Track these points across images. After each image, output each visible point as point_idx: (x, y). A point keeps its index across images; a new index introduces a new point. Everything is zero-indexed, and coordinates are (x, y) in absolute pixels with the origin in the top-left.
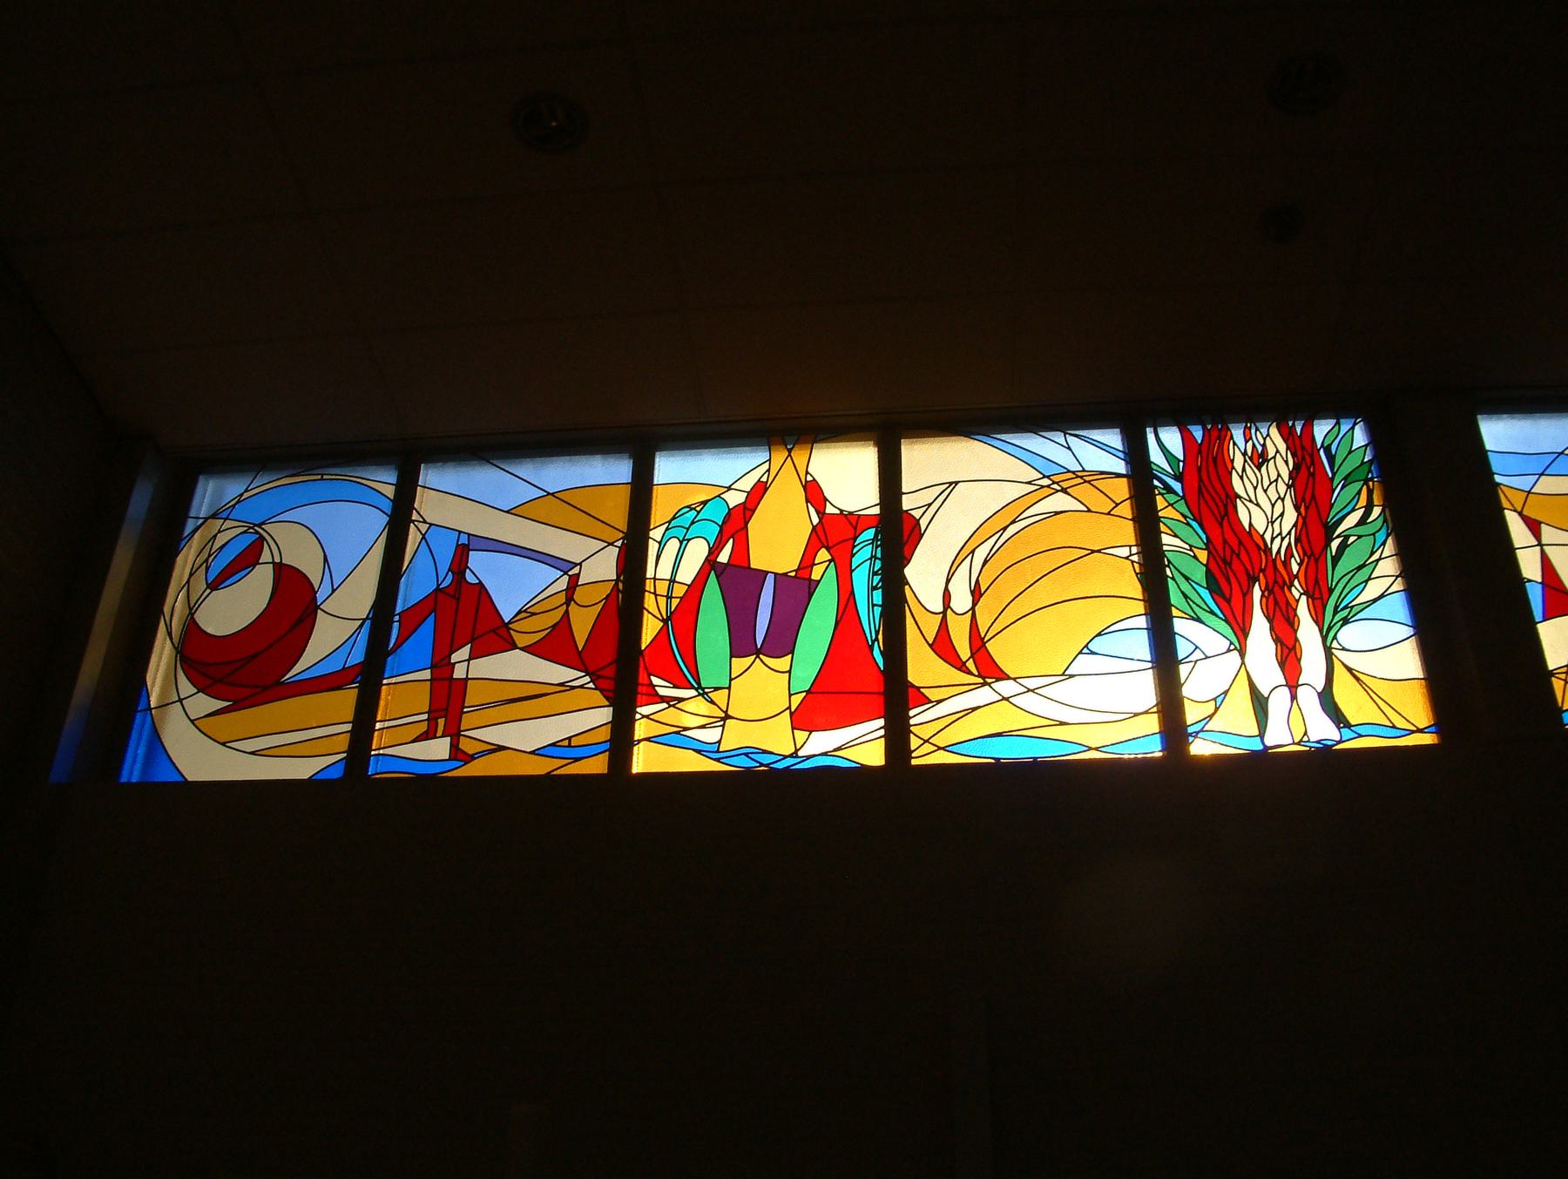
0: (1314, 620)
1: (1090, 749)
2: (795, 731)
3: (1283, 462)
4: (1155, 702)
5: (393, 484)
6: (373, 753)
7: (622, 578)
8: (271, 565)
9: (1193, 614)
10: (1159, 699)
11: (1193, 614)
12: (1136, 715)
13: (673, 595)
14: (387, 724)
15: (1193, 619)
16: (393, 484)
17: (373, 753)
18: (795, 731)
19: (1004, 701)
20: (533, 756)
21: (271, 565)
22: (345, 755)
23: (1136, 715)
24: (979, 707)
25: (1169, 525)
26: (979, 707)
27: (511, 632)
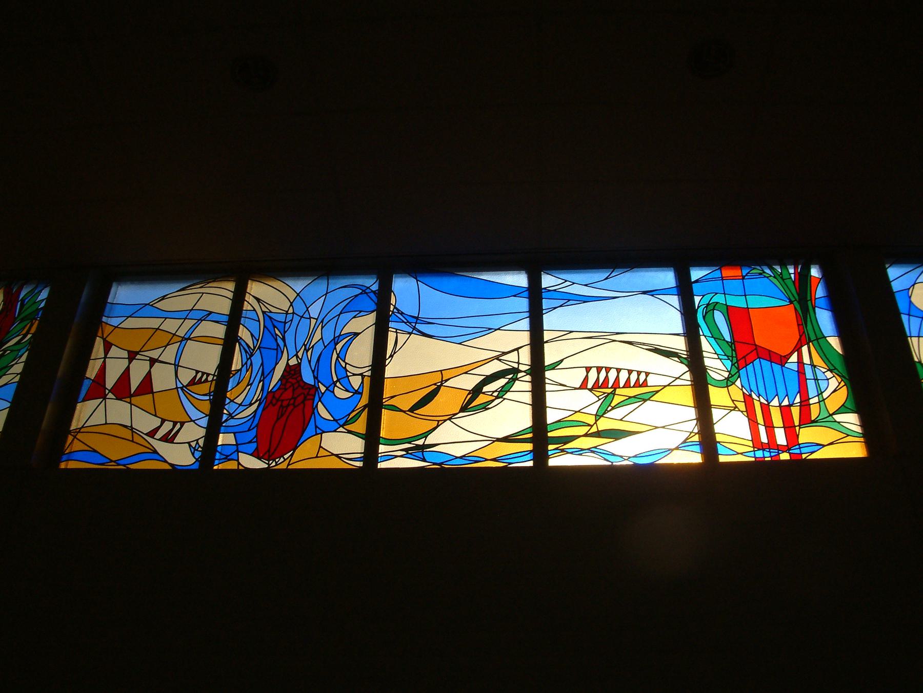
0: (422, 461)
1: (486, 460)
2: (155, 437)
3: (596, 445)
4: (715, 426)
5: (527, 312)
6: (380, 455)
7: (391, 313)
8: (154, 391)
9: (465, 458)
10: (699, 429)
11: (465, 458)
12: (663, 427)
13: (398, 334)
14: (383, 454)
15: (464, 456)
16: (527, 312)
17: (380, 455)
18: (155, 437)
19: (508, 390)
20: (486, 458)
21: (154, 391)
22: (363, 455)
23: (663, 427)
24: (396, 396)
25: (475, 455)
26: (396, 396)
27: (115, 398)
